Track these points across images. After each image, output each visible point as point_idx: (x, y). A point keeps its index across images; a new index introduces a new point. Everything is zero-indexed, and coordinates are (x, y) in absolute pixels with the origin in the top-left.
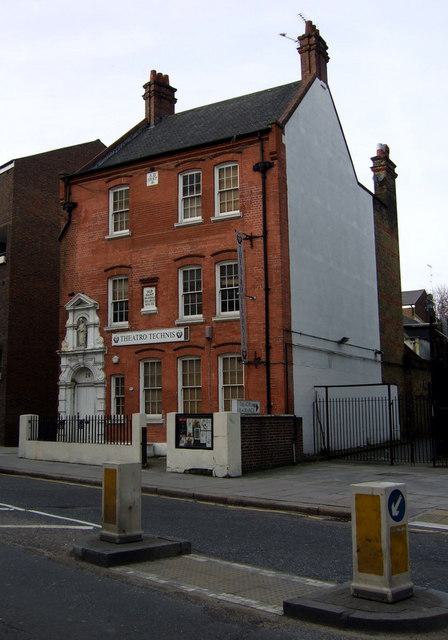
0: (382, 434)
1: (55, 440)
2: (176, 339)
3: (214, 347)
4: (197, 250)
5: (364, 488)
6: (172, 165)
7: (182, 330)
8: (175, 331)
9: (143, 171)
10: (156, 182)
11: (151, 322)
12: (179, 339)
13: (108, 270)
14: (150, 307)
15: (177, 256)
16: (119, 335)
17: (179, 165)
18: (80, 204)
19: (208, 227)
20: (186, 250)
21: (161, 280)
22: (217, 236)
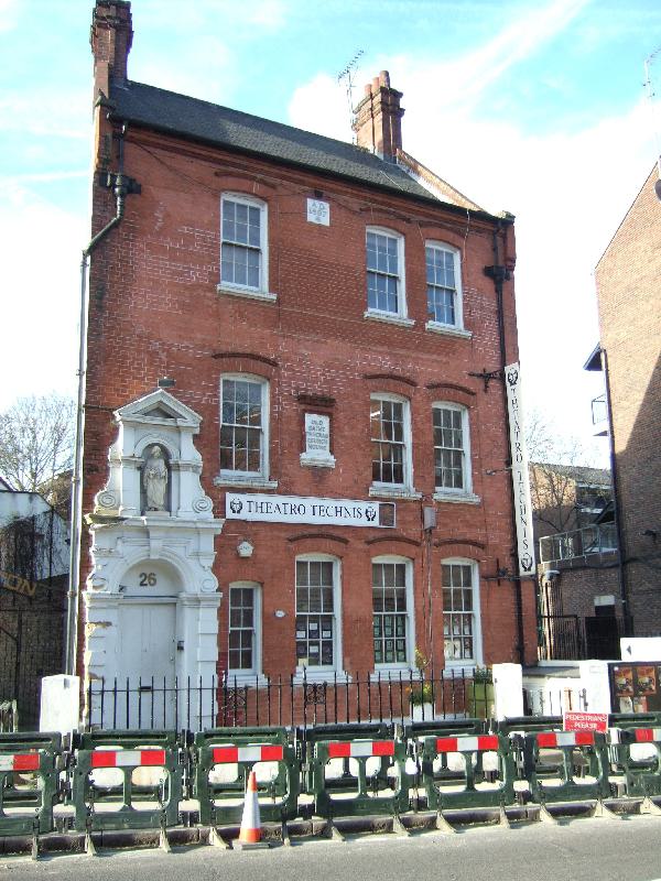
0: (537, 708)
1: (524, 675)
2: (363, 522)
3: (436, 545)
4: (408, 368)
5: (135, 861)
6: (355, 204)
7: (376, 506)
8: (363, 505)
9: (298, 188)
10: (311, 218)
11: (318, 482)
12: (371, 524)
13: (222, 356)
14: (318, 453)
15: (370, 371)
16: (244, 498)
17: (368, 210)
18: (144, 186)
19: (414, 338)
20: (386, 364)
21: (339, 404)
22: (435, 357)
